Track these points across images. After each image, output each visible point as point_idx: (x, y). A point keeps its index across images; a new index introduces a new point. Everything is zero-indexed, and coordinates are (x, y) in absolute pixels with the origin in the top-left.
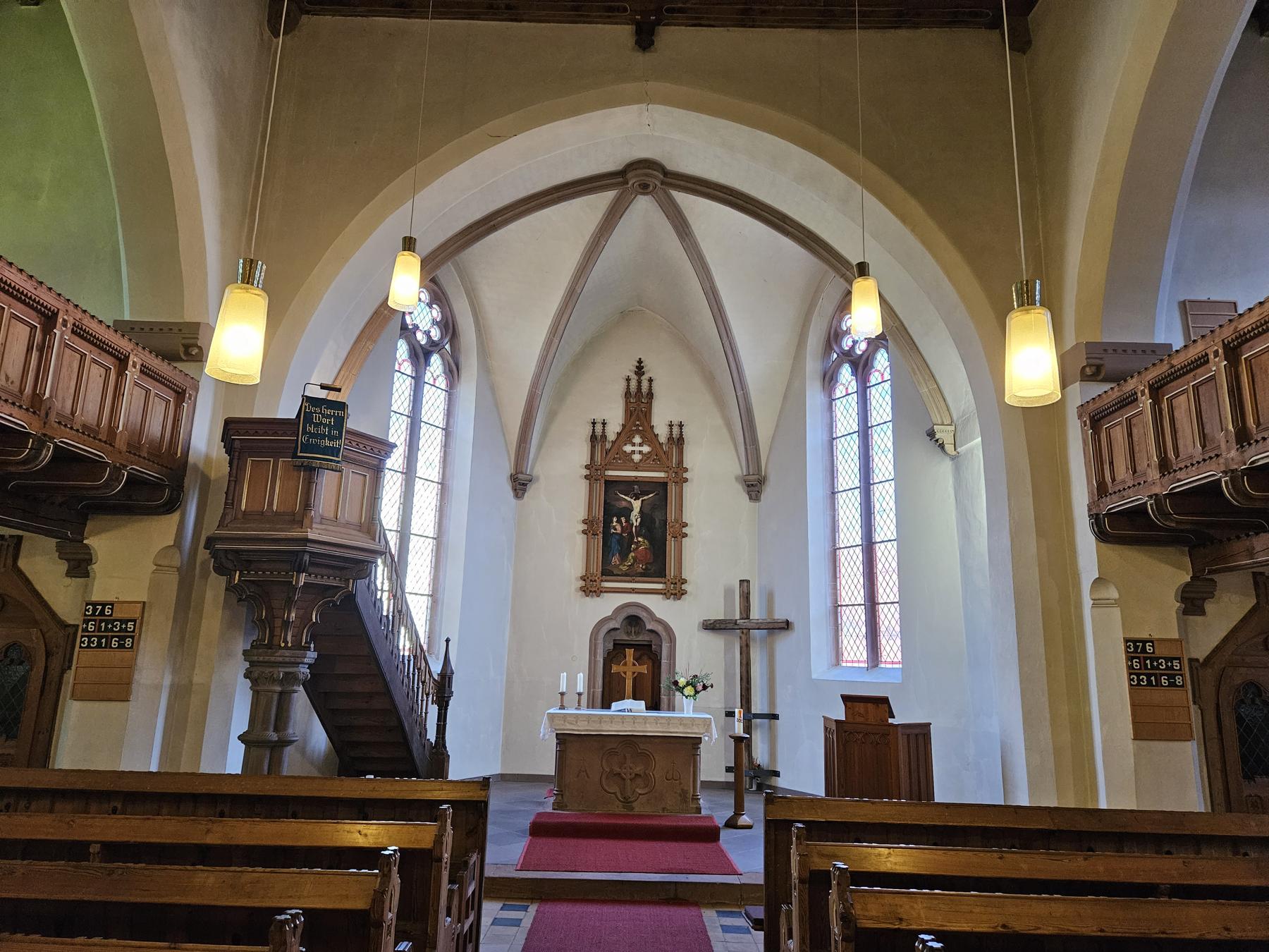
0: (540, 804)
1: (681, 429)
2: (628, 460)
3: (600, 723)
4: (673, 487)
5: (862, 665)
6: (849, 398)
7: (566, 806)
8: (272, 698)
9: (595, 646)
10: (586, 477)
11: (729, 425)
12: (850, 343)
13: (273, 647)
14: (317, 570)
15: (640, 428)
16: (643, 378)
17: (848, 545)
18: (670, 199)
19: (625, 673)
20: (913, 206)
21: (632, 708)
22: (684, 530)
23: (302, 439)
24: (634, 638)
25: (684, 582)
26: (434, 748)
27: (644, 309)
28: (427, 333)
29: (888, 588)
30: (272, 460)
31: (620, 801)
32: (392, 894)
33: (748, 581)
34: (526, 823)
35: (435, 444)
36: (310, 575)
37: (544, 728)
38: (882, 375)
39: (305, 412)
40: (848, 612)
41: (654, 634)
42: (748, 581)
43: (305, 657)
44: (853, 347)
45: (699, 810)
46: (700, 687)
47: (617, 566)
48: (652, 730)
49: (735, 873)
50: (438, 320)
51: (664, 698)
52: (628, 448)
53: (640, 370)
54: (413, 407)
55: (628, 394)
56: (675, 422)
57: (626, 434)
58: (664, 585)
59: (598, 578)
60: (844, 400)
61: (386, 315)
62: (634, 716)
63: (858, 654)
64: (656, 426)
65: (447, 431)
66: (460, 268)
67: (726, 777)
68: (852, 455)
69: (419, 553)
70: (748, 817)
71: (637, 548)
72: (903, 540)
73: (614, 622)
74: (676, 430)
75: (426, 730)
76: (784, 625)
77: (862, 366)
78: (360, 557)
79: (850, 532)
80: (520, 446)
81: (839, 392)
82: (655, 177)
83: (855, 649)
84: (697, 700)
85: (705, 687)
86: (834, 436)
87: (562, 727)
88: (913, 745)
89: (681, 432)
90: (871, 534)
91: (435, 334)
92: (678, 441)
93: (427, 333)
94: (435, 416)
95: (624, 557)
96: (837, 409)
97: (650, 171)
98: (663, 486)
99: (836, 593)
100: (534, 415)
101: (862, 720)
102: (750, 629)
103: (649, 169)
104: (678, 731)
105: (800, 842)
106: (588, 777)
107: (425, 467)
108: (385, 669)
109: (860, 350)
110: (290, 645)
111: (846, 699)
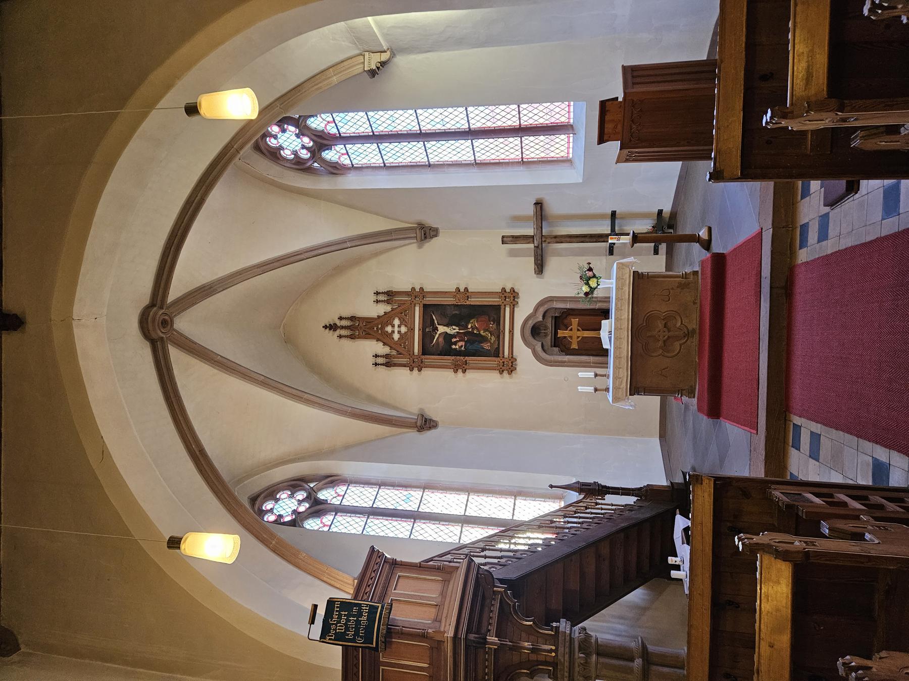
0: (687, 407)
1: (380, 293)
2: (406, 336)
3: (620, 357)
4: (427, 299)
5: (571, 139)
6: (350, 152)
7: (691, 386)
8: (603, 663)
9: (556, 362)
10: (420, 370)
11: (376, 254)
12: (304, 151)
13: (555, 661)
14: (485, 623)
15: (380, 327)
16: (339, 324)
17: (472, 152)
18: (182, 299)
19: (578, 337)
20: (157, 76)
21: (607, 331)
22: (462, 290)
23: (360, 642)
24: (549, 331)
25: (504, 290)
26: (641, 498)
27: (283, 324)
28: (300, 502)
29: (506, 116)
30: (381, 667)
31: (687, 341)
32: (779, 542)
33: (503, 237)
34: (705, 421)
35: (391, 495)
36: (489, 631)
37: (626, 405)
38: (328, 122)
39: (335, 640)
40: (527, 152)
41: (546, 314)
42: (503, 237)
43: (565, 632)
44: (308, 149)
45: (695, 273)
46: (590, 274)
47: (492, 345)
48: (627, 314)
49: (760, 235)
50: (290, 493)
51: (598, 306)
52: (396, 336)
53: (332, 327)
54: (360, 514)
55: (352, 337)
56: (374, 298)
57: (385, 338)
58: (507, 306)
59: (501, 360)
60: (352, 156)
61: (276, 542)
62: (615, 329)
63: (562, 143)
64: (378, 313)
65: (381, 484)
66: (246, 476)
67: (662, 255)
68: (397, 149)
69: (481, 507)
70: (700, 231)
71: (477, 328)
72: (465, 101)
73: (537, 347)
74: (381, 298)
75: (626, 505)
76: (539, 206)
77: (322, 141)
78: (473, 582)
79: (460, 151)
80: (394, 424)
81: (345, 161)
82: (156, 314)
83: (559, 146)
84: (601, 276)
85: (590, 269)
86: (383, 165)
87: (625, 390)
88: (642, 80)
89: (382, 293)
90: (462, 132)
91: (301, 495)
92: (390, 296)
93: (300, 502)
94: (369, 495)
95: (484, 339)
96: (360, 163)
97: (149, 318)
98: (426, 307)
99: (512, 162)
100: (368, 413)
101: (619, 127)
102: (542, 235)
103: (148, 319)
104: (628, 290)
105: (790, 113)
106: (667, 368)
107: (411, 503)
108: (576, 546)
109: (310, 143)
110: (554, 648)
111: (601, 140)
